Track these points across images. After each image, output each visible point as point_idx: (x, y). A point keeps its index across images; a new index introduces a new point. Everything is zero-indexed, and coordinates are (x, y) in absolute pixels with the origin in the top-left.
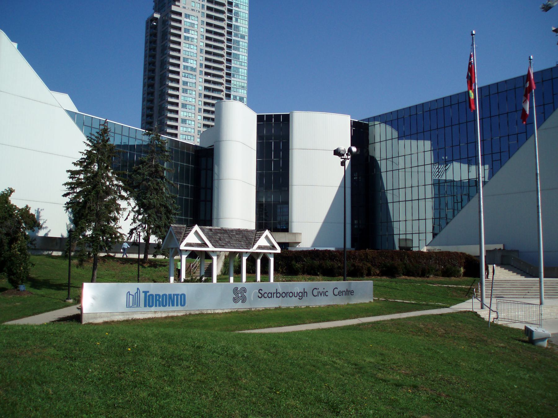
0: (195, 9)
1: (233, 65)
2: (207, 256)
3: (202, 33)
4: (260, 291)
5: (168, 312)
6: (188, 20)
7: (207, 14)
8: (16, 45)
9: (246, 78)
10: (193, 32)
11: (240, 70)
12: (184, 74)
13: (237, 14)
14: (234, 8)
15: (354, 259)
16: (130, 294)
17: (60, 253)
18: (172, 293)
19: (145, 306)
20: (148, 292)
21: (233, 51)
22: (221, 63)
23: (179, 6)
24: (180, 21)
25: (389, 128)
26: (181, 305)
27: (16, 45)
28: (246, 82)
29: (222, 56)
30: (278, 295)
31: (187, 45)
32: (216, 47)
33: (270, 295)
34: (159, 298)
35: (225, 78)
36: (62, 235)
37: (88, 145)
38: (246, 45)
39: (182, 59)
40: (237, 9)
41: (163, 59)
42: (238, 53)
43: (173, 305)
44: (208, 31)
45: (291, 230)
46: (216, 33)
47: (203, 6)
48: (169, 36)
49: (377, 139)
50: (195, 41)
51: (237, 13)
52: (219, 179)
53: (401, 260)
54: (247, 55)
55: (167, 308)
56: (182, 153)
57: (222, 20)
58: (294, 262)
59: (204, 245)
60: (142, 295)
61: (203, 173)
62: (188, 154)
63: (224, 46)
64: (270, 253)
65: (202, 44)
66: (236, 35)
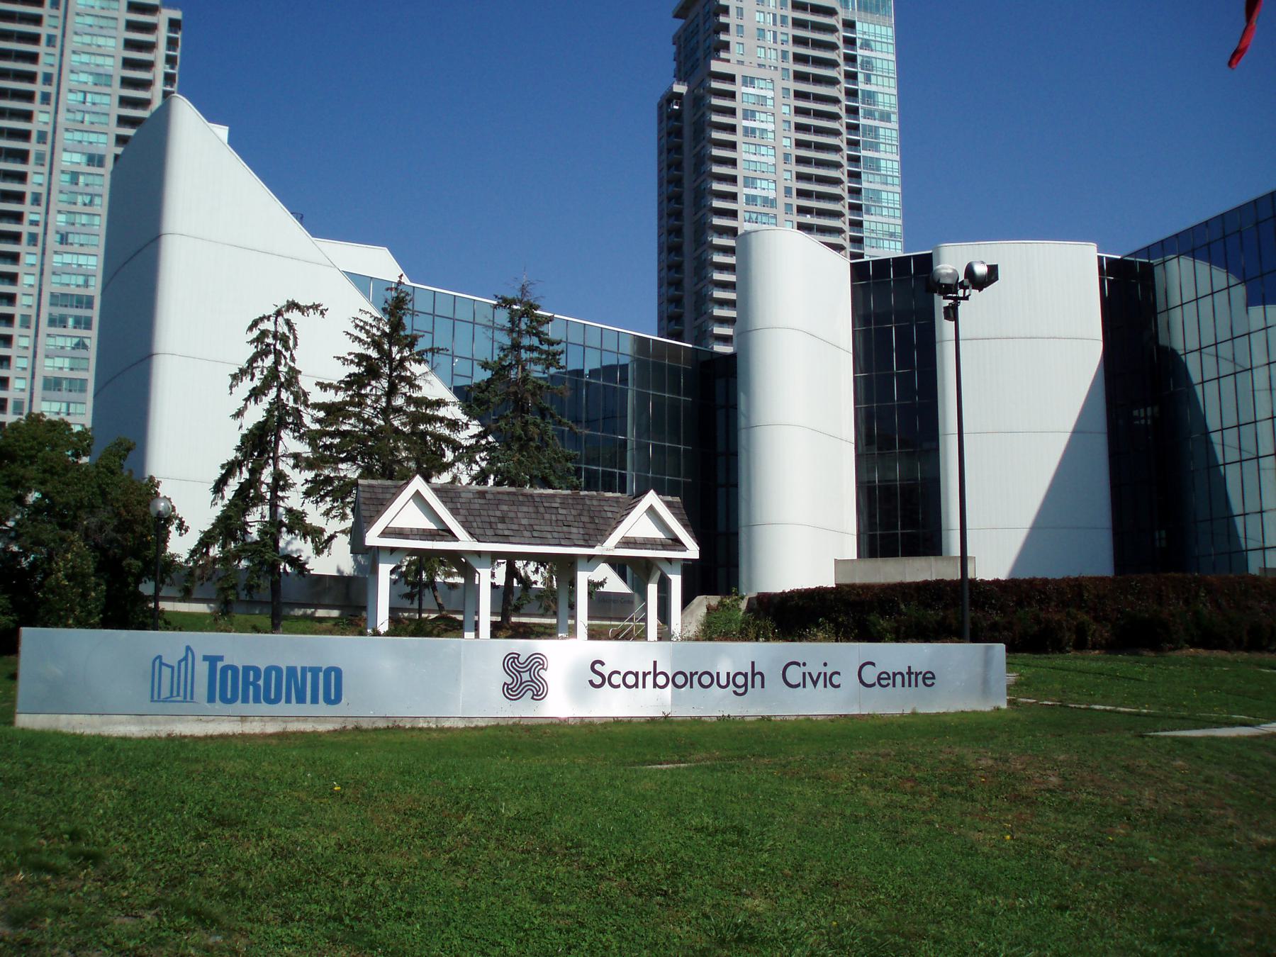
0: (767, 63)
1: (865, 185)
2: (463, 563)
3: (787, 117)
4: (598, 667)
5: (286, 718)
6: (750, 90)
7: (795, 72)
8: (223, 132)
9: (898, 213)
10: (763, 117)
11: (884, 195)
12: (747, 215)
13: (868, 64)
14: (860, 52)
15: (1040, 602)
16: (161, 664)
17: (335, 613)
18: (299, 665)
19: (211, 699)
20: (221, 658)
21: (863, 153)
22: (837, 182)
23: (728, 61)
24: (732, 95)
25: (1203, 267)
26: (328, 701)
27: (223, 132)
28: (900, 222)
29: (838, 165)
30: (661, 680)
31: (752, 148)
32: (820, 147)
33: (631, 680)
34: (257, 677)
35: (848, 216)
36: (339, 570)
37: (357, 338)
38: (895, 134)
39: (740, 180)
40: (867, 53)
41: (699, 186)
42: (875, 155)
43: (301, 700)
44: (799, 111)
45: (948, 552)
46: (819, 114)
47: (784, 53)
48: (708, 129)
49: (1175, 299)
50: (771, 135)
51: (868, 63)
52: (749, 427)
53: (1187, 602)
54: (898, 158)
55: (281, 708)
56: (659, 367)
57: (833, 82)
58: (872, 618)
59: (447, 534)
60: (202, 669)
61: (720, 415)
62: (675, 372)
63: (840, 141)
64: (669, 560)
65: (786, 142)
66: (869, 114)
